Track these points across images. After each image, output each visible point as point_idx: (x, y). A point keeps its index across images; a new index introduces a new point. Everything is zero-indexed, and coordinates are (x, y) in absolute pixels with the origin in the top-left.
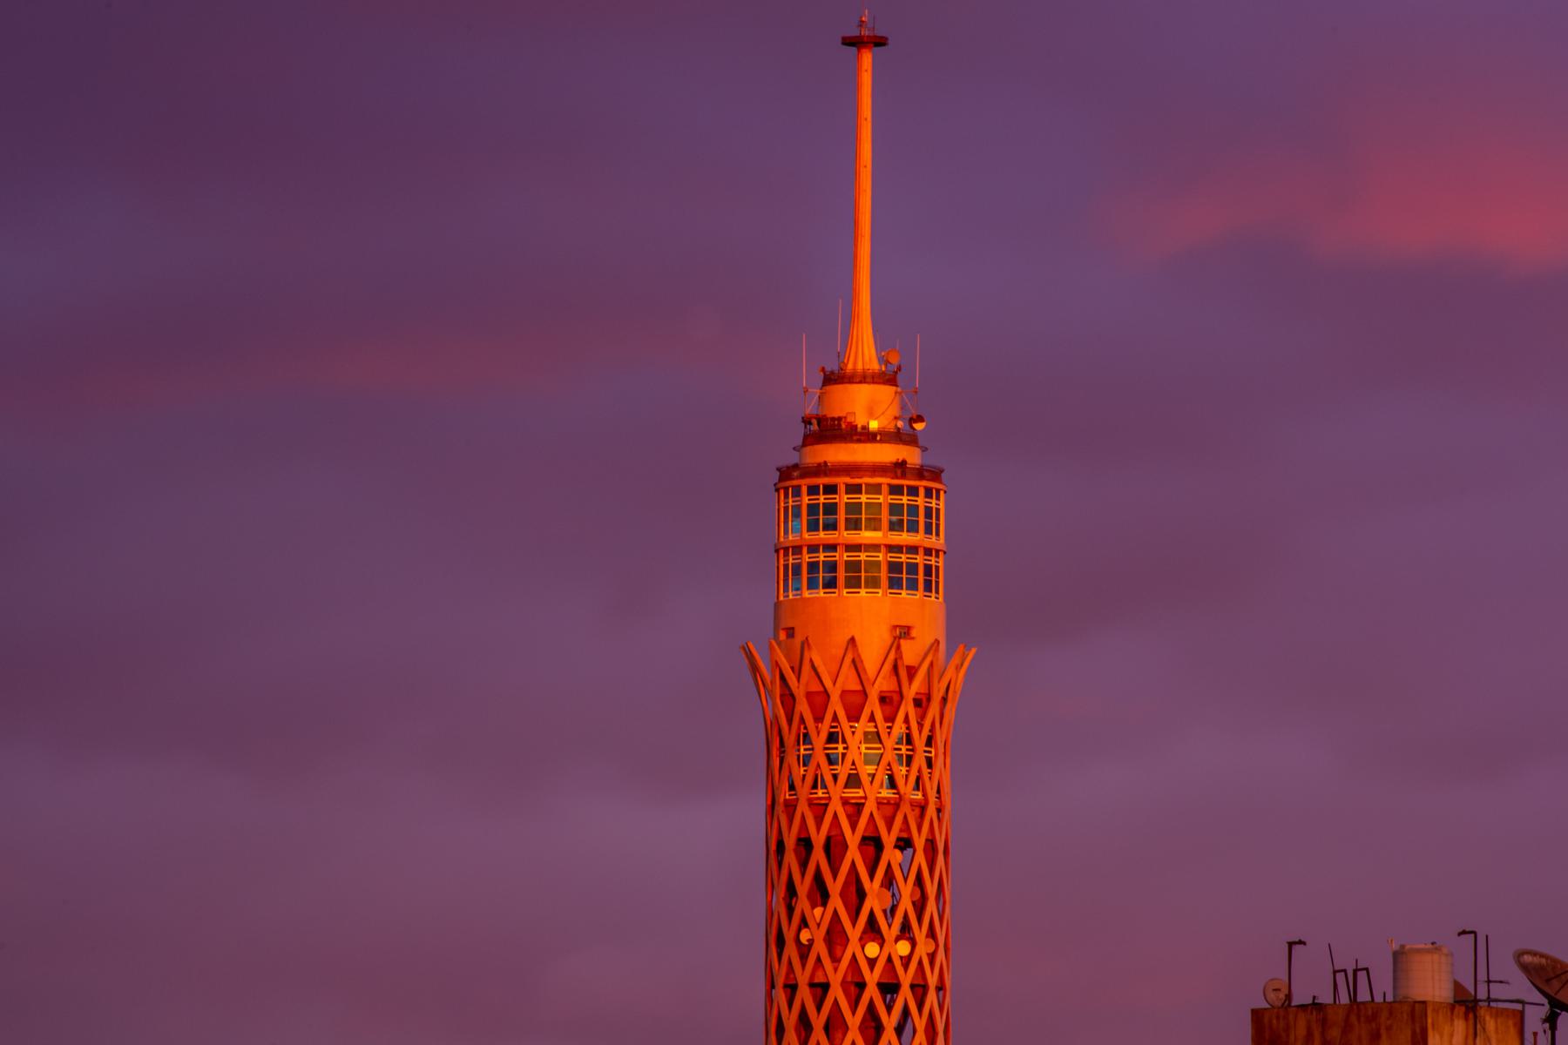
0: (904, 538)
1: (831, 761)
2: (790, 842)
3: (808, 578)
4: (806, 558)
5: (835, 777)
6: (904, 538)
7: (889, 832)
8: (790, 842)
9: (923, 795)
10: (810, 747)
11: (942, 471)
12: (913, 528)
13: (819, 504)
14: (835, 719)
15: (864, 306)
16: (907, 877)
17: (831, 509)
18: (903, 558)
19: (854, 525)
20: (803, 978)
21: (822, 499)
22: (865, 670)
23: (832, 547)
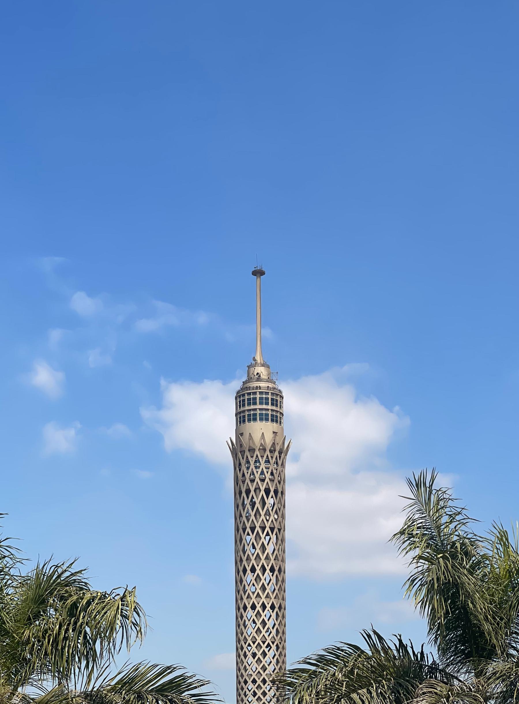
0: (264, 406)
1: (256, 467)
2: (243, 490)
3: (248, 419)
4: (247, 413)
5: (257, 472)
6: (264, 406)
7: (263, 495)
8: (243, 490)
9: (280, 479)
10: (249, 464)
11: (243, 382)
12: (267, 404)
13: (251, 398)
14: (257, 456)
15: (259, 335)
16: (117, 633)
17: (255, 399)
18: (264, 412)
19: (249, 404)
20: (248, 525)
21: (264, 396)
22: (266, 443)
23: (255, 409)
